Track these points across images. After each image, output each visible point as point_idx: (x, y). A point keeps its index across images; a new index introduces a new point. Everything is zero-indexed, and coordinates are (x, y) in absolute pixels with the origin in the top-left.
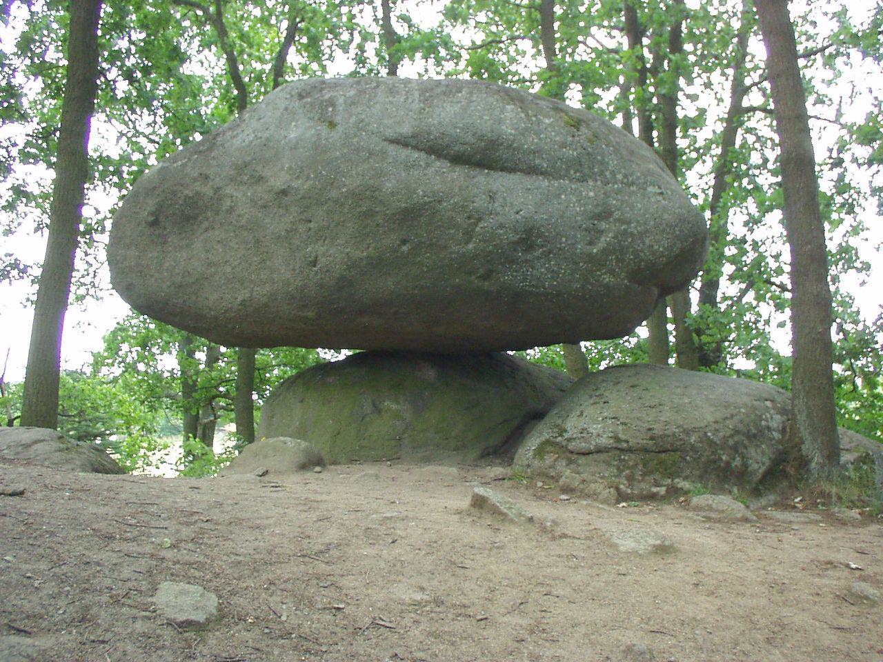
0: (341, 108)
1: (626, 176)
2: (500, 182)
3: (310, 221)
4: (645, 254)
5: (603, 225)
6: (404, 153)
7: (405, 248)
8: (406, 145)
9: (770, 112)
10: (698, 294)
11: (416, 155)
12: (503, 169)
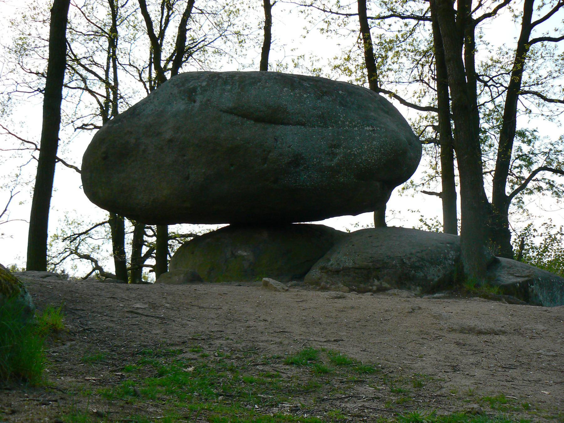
0: (396, 292)
1: (350, 122)
2: (280, 130)
3: (185, 156)
4: (363, 165)
5: (337, 151)
6: (229, 117)
7: (232, 168)
8: (231, 113)
9: (481, 76)
10: (458, 218)
11: (236, 118)
12: (283, 123)
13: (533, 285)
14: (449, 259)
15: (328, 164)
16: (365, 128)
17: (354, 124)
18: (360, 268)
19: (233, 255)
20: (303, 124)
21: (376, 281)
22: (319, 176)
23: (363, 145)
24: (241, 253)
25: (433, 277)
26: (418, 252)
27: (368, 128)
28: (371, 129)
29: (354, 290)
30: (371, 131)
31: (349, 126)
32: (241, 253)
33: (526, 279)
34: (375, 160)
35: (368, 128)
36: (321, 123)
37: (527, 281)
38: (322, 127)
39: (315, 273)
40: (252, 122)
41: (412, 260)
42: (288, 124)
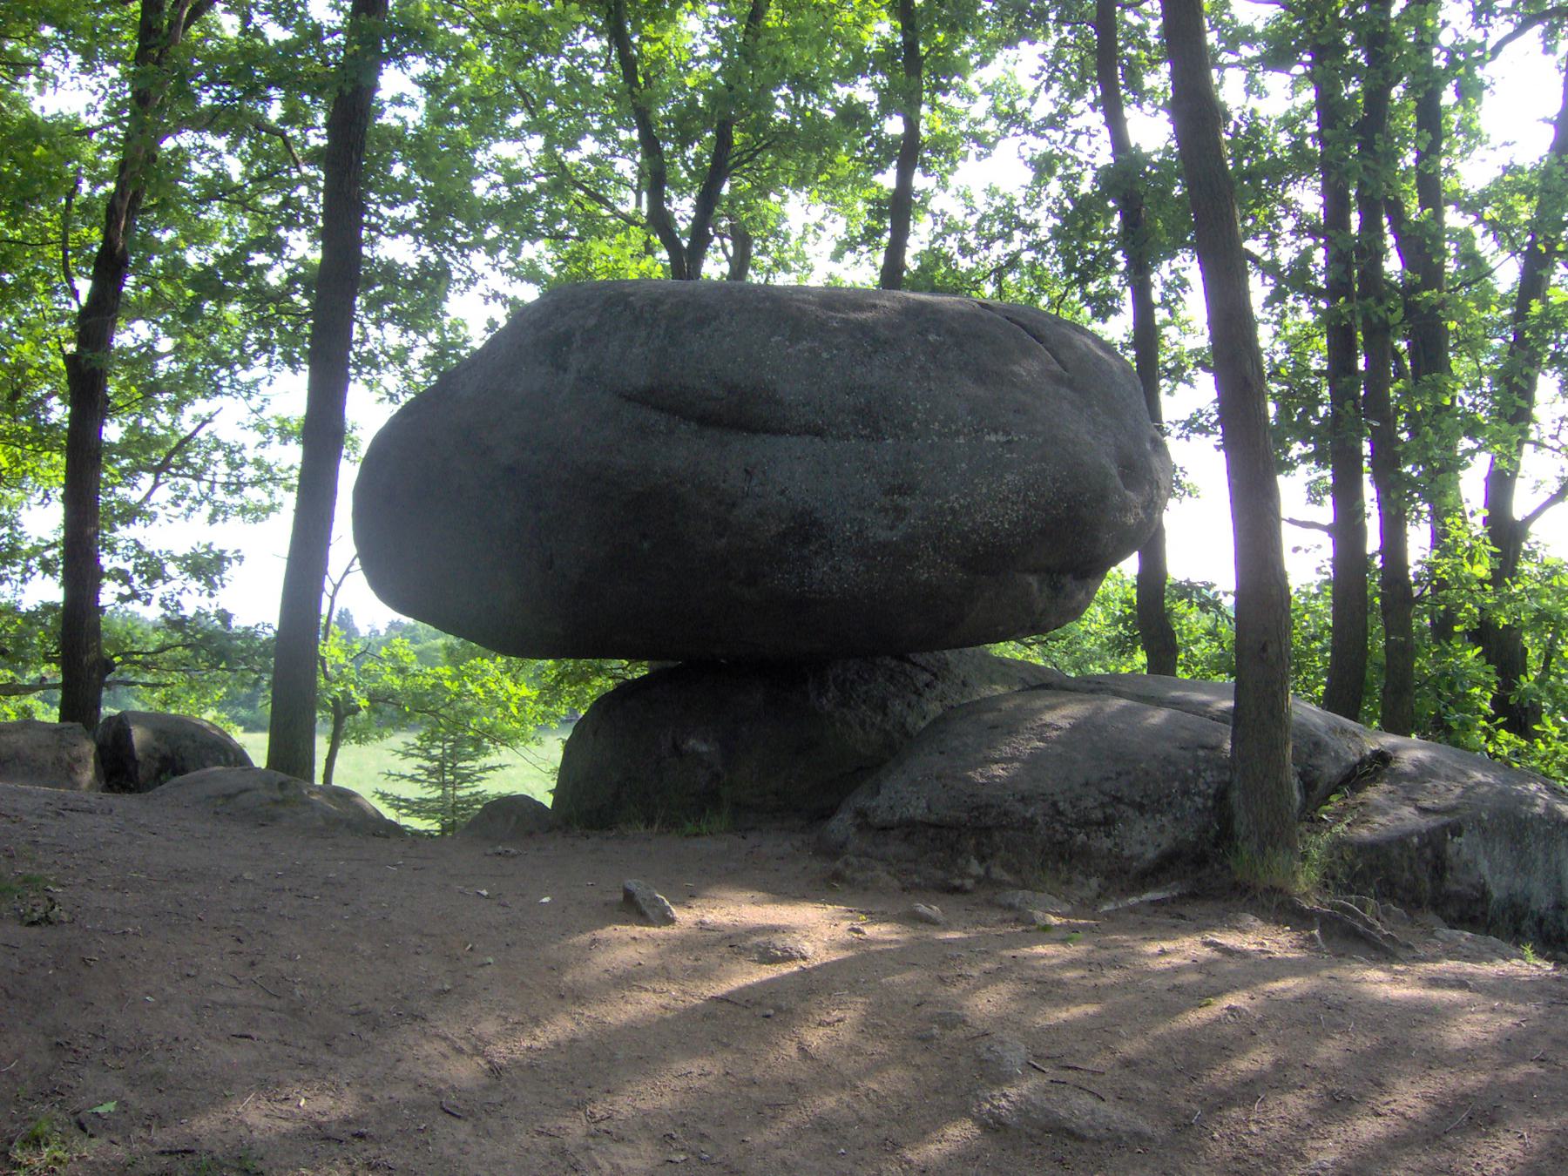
5: (908, 502)
7: (646, 545)
13: (1460, 836)
14: (1199, 794)
15: (883, 535)
16: (987, 438)
17: (954, 427)
18: (938, 826)
19: (676, 749)
20: (819, 433)
21: (974, 862)
22: (861, 568)
23: (976, 485)
24: (694, 744)
25: (1138, 849)
26: (1108, 779)
27: (993, 438)
28: (1003, 439)
29: (916, 887)
30: (1002, 445)
31: (940, 435)
32: (694, 744)
33: (1446, 819)
34: (1010, 523)
35: (993, 438)
36: (865, 428)
37: (1444, 826)
38: (867, 438)
39: (841, 825)
40: (694, 426)
41: (1082, 805)
42: (779, 432)
